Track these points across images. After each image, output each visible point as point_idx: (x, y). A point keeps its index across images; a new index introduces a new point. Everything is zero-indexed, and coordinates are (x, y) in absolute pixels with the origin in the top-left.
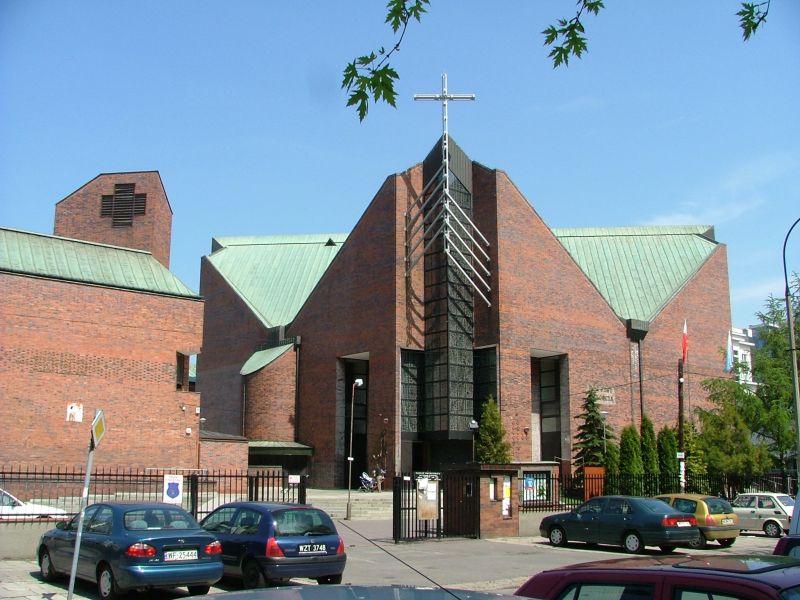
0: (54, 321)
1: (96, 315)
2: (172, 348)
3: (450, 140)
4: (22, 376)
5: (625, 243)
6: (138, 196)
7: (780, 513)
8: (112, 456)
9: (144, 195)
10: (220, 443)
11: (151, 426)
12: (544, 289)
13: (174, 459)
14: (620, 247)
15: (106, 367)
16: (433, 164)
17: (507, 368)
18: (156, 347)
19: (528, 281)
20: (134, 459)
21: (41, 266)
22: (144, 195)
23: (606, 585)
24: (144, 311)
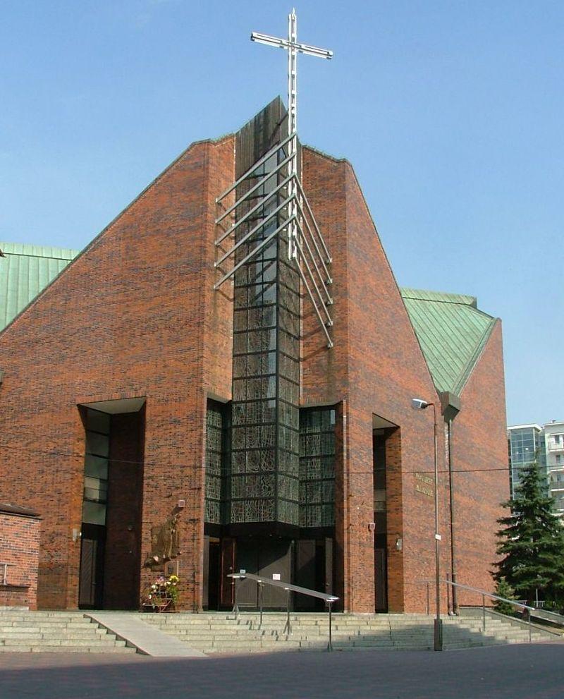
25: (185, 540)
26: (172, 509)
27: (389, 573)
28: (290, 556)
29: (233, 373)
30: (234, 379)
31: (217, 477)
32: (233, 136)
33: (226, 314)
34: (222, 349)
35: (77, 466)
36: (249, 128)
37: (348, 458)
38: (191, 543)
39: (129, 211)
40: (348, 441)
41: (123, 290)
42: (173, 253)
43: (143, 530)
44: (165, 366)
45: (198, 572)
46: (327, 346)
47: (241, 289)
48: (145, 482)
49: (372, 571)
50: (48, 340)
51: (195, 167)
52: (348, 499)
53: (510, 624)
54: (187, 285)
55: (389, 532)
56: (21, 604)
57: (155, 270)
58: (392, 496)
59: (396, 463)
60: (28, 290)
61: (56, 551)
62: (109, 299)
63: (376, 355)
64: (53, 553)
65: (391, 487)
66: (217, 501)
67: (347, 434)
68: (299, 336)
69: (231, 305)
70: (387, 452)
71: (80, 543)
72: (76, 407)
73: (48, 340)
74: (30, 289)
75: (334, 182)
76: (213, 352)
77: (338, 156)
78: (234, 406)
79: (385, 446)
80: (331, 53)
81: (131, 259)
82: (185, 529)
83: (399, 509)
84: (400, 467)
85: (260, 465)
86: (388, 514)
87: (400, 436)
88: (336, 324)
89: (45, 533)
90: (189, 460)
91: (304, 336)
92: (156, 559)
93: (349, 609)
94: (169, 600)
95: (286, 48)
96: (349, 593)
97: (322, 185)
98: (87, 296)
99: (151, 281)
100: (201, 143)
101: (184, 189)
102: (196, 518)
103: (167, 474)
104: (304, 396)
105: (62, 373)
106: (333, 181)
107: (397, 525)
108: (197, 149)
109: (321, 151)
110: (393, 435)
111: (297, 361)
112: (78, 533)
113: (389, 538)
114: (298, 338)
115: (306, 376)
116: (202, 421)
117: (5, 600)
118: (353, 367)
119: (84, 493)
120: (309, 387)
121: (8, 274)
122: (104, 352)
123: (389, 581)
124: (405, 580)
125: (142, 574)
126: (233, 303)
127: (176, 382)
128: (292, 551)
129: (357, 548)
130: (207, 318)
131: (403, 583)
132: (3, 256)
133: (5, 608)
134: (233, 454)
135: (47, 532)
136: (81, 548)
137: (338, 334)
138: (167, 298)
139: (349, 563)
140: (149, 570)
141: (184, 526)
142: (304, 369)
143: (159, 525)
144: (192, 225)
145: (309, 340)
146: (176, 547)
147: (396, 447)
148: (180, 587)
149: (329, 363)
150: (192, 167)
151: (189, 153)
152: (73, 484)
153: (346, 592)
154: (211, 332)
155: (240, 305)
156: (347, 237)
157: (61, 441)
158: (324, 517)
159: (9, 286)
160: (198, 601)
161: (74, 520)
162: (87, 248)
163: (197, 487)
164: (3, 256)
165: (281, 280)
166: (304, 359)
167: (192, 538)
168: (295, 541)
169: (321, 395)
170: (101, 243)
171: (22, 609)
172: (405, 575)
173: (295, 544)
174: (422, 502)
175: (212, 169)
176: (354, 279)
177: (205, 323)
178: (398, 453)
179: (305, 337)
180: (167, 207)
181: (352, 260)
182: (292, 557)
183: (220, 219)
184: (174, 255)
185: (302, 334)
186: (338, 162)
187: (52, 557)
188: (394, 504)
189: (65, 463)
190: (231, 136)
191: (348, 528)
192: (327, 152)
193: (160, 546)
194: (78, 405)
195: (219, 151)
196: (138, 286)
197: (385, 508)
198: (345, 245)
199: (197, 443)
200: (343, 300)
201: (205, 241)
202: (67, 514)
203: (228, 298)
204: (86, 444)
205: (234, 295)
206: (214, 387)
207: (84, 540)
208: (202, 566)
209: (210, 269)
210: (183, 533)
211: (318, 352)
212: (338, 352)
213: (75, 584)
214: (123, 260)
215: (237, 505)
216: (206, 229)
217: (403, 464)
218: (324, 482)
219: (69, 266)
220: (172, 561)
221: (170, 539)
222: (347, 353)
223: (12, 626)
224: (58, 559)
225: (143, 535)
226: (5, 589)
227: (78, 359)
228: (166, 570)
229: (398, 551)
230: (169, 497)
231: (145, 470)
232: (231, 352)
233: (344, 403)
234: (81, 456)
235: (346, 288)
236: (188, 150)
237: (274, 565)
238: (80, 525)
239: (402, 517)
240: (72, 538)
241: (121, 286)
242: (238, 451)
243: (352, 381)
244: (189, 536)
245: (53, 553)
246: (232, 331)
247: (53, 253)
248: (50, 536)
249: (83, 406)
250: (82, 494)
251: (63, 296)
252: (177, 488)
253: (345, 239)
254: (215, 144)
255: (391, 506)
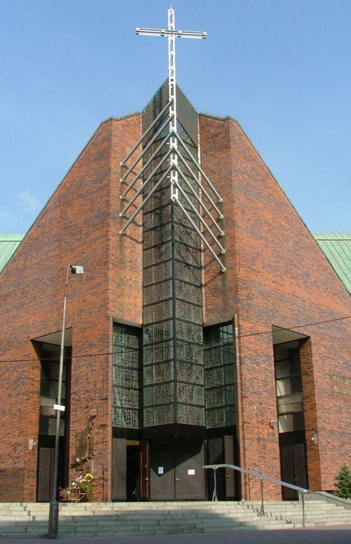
3: (180, 95)
5: (338, 248)
7: (114, 398)
12: (283, 259)
14: (332, 249)
16: (159, 101)
17: (249, 345)
19: (267, 247)
23: (225, 489)
25: (97, 443)
26: (89, 417)
27: (308, 465)
28: (203, 453)
29: (143, 301)
30: (144, 306)
31: (135, 389)
32: (140, 114)
33: (136, 254)
34: (130, 283)
35: (31, 388)
36: (151, 106)
37: (241, 364)
38: (101, 445)
39: (63, 184)
40: (240, 350)
41: (59, 246)
42: (89, 210)
43: (70, 437)
44: (84, 301)
45: (107, 470)
46: (221, 271)
47: (148, 232)
48: (72, 396)
49: (277, 463)
51: (103, 141)
52: (242, 400)
53: (343, 508)
54: (97, 234)
55: (306, 429)
57: (77, 226)
58: (307, 397)
59: (309, 369)
61: (17, 459)
62: (50, 254)
63: (275, 276)
65: (306, 389)
66: (135, 409)
67: (240, 343)
68: (201, 266)
69: (140, 247)
70: (301, 360)
71: (37, 451)
72: (31, 342)
75: (222, 137)
76: (121, 284)
77: (223, 116)
78: (144, 329)
79: (299, 355)
80: (205, 33)
81: (64, 220)
82: (97, 434)
83: (313, 408)
84: (312, 371)
85: (163, 376)
86: (305, 413)
87: (310, 345)
88: (227, 251)
89: (11, 444)
90: (100, 375)
91: (205, 265)
92: (78, 460)
93: (246, 498)
94: (82, 495)
95: (166, 35)
96: (246, 483)
97: (213, 141)
98: (37, 255)
99: (76, 235)
100: (107, 121)
101: (96, 160)
102: (104, 423)
103: (85, 389)
104: (207, 316)
105: (22, 316)
106: (221, 136)
107: (313, 422)
108: (104, 127)
109: (205, 113)
110: (305, 344)
111: (201, 286)
113: (307, 434)
114: (200, 268)
115: (207, 299)
116: (108, 342)
118: (244, 286)
119: (270, 425)
120: (210, 307)
122: (47, 296)
123: (309, 473)
124: (322, 471)
125: (70, 473)
126: (141, 245)
127: (91, 313)
128: (205, 449)
129: (255, 443)
130: (112, 258)
131: (320, 473)
134: (144, 368)
136: (38, 455)
137: (229, 260)
138: (85, 246)
139: (245, 456)
140: (74, 470)
141: (96, 431)
142: (206, 293)
143: (81, 431)
144: (101, 186)
145: (208, 268)
146: (91, 449)
147: (308, 354)
148: (94, 483)
149: (224, 284)
150: (101, 141)
151: (99, 131)
152: (28, 403)
153: (243, 483)
154: (117, 269)
155: (147, 246)
156: (233, 179)
157: (21, 370)
158: (228, 418)
160: (107, 494)
161: (30, 432)
162: (38, 218)
163: (105, 397)
165: (175, 220)
166: (206, 285)
167: (102, 441)
168: (207, 440)
169: (219, 313)
170: (46, 212)
172: (322, 466)
173: (208, 442)
174: (342, 402)
175: (115, 140)
176: (243, 212)
177: (110, 261)
178: (310, 359)
179: (205, 267)
180: (86, 175)
181: (240, 198)
182: (204, 452)
183: (124, 177)
184: (90, 212)
185: (203, 264)
186: (224, 120)
188: (310, 403)
189: (23, 387)
190: (137, 114)
191: (243, 426)
192: (215, 115)
193: (81, 449)
194: (32, 341)
195: (123, 126)
196: (68, 241)
197: (303, 409)
198: (231, 185)
199: (105, 360)
200: (232, 231)
201: (109, 196)
202: (24, 427)
203: (137, 241)
204: (41, 371)
205: (143, 238)
206: (121, 314)
207: (41, 449)
208: (110, 464)
209: (114, 219)
210: (96, 437)
211: (215, 277)
212: (230, 275)
214: (59, 222)
215: (147, 411)
216: (110, 186)
217: (315, 369)
218: (227, 388)
220: (89, 461)
221: (86, 443)
222: (236, 275)
225: (71, 441)
227: (31, 304)
228: (85, 470)
229: (314, 445)
230: (87, 407)
231: (72, 387)
232: (141, 284)
233: (236, 318)
234: (36, 381)
235: (234, 220)
236: (98, 129)
237: (189, 461)
239: (316, 414)
240: (28, 447)
241: (58, 243)
242: (148, 365)
243: (243, 297)
244: (100, 440)
246: (142, 267)
248: (14, 446)
251: (24, 258)
252: (92, 400)
253: (231, 181)
254: (117, 120)
255: (307, 406)
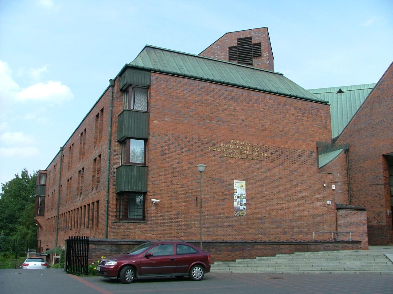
0: (232, 117)
1: (262, 113)
2: (313, 139)
4: (214, 161)
6: (255, 45)
8: (280, 223)
9: (259, 44)
10: (349, 212)
11: (304, 199)
13: (321, 225)
15: (272, 153)
18: (304, 138)
20: (295, 225)
21: (217, 77)
22: (259, 44)
24: (293, 111)
50: (365, 128)
56: (359, 249)
60: (356, 106)
64: (380, 221)
73: (365, 128)
74: (357, 105)
112: (390, 211)
117: (351, 247)
119: (391, 193)
121: (346, 100)
132: (344, 93)
133: (351, 251)
135: (376, 212)
159: (348, 105)
164: (344, 93)
171: (359, 251)
187: (379, 222)
213: (391, 234)
219: (372, 91)
223: (351, 261)
224: (382, 223)
226: (350, 243)
238: (391, 208)
245: (380, 221)
247: (370, 86)
249: (385, 155)
250: (390, 194)
